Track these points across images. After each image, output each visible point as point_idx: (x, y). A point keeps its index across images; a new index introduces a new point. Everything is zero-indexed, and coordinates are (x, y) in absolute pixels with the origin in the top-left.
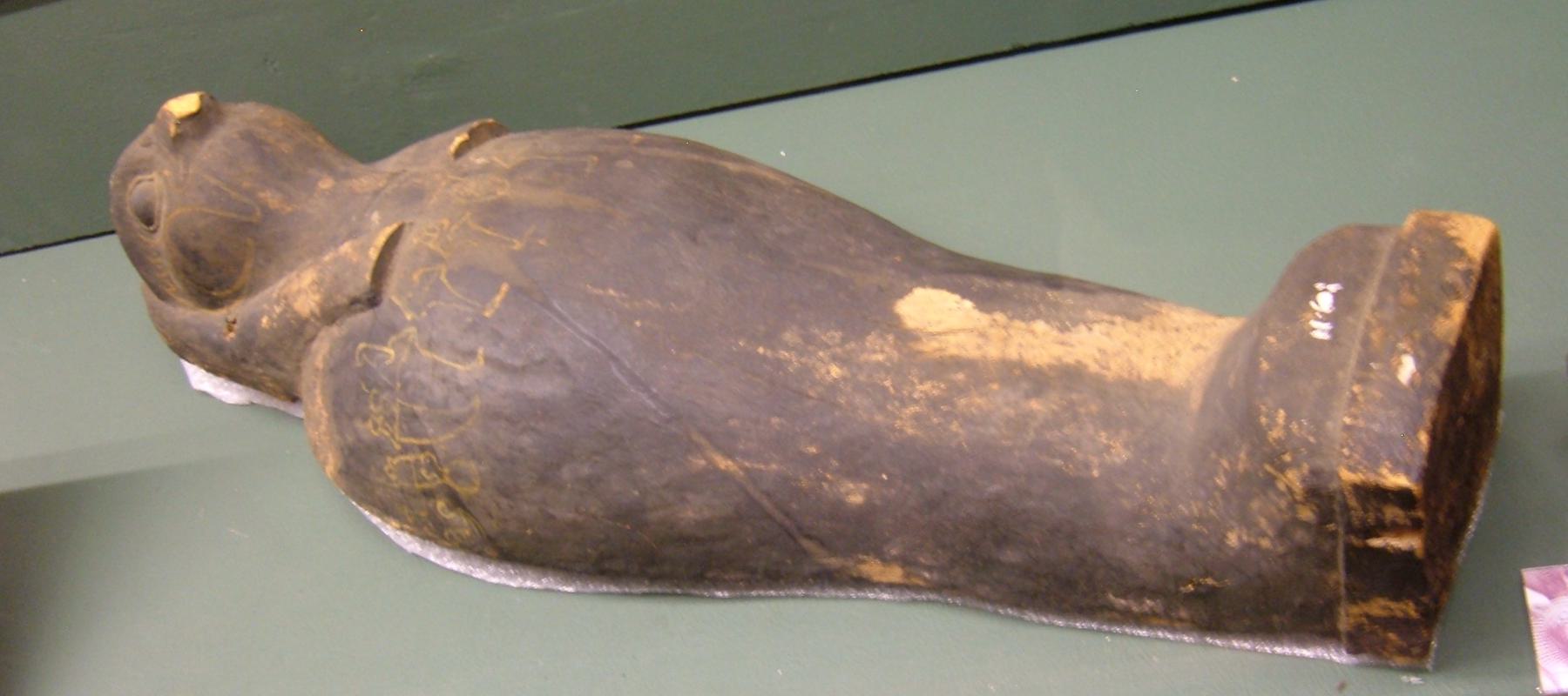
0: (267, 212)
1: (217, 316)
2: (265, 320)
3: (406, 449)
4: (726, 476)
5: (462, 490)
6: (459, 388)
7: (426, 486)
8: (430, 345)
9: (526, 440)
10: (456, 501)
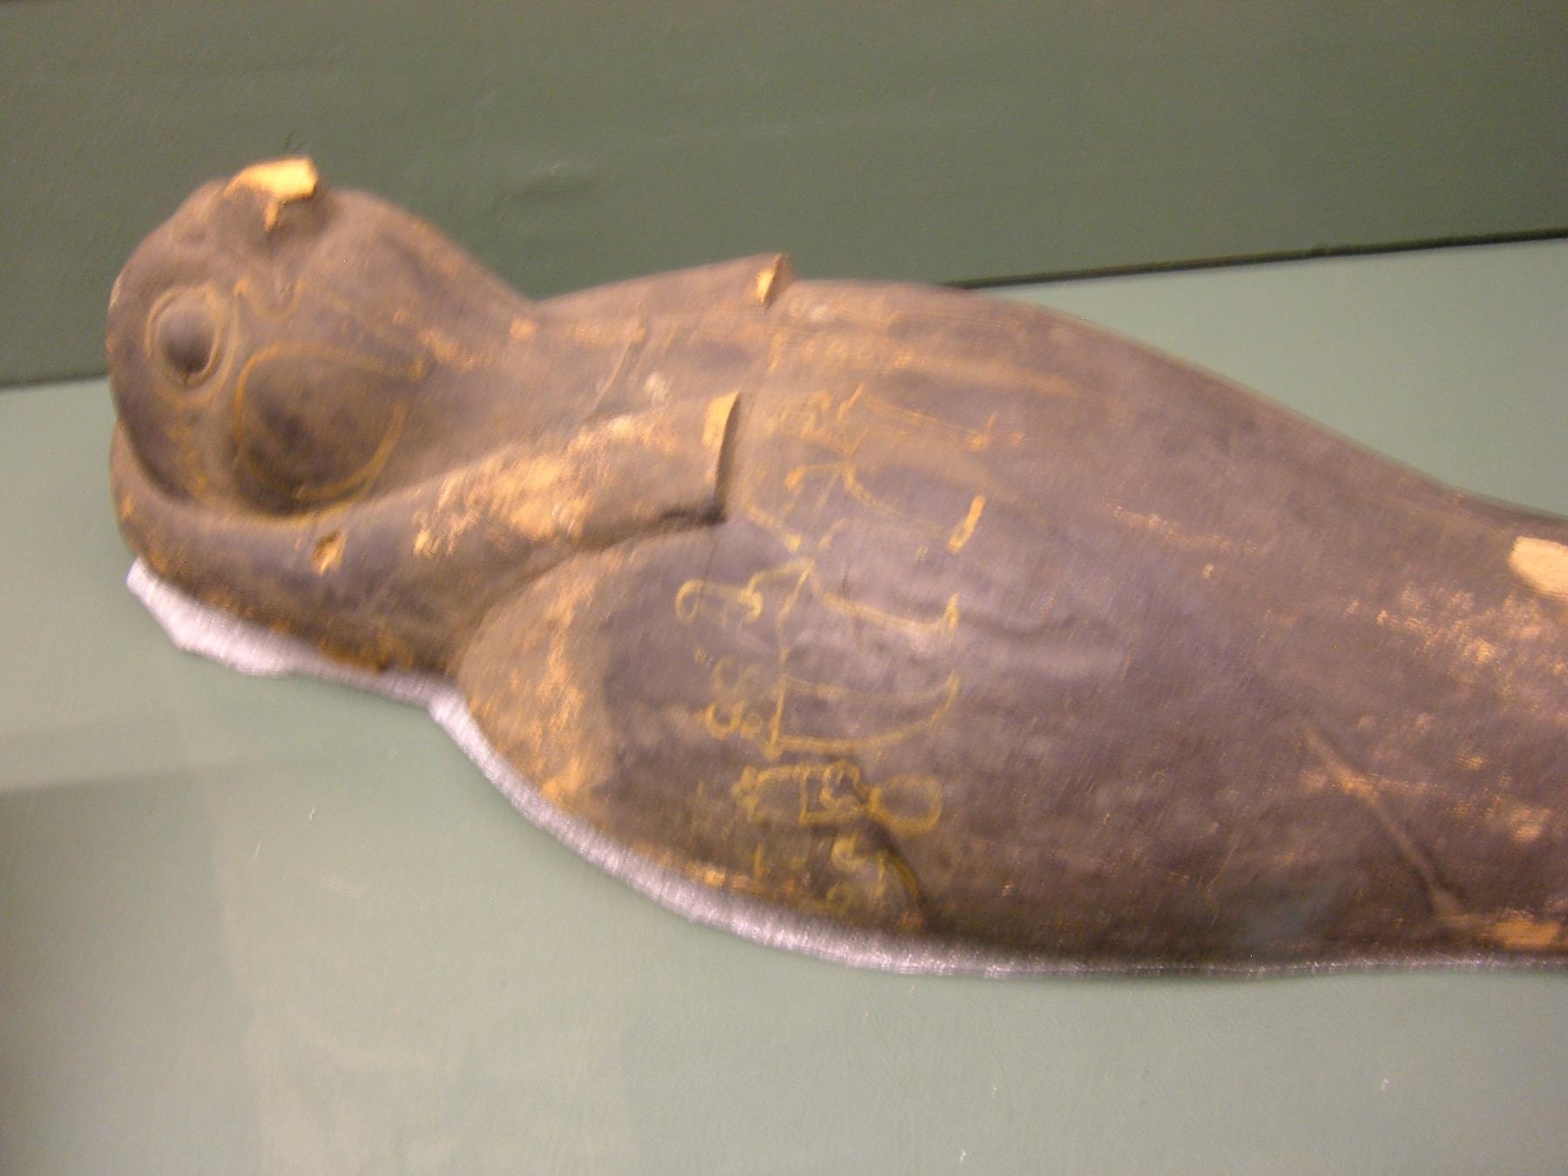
0: (433, 365)
1: (293, 531)
2: (422, 541)
3: (790, 758)
4: (1352, 802)
5: (899, 824)
6: (914, 661)
7: (824, 818)
8: (845, 590)
9: (1040, 746)
10: (880, 840)
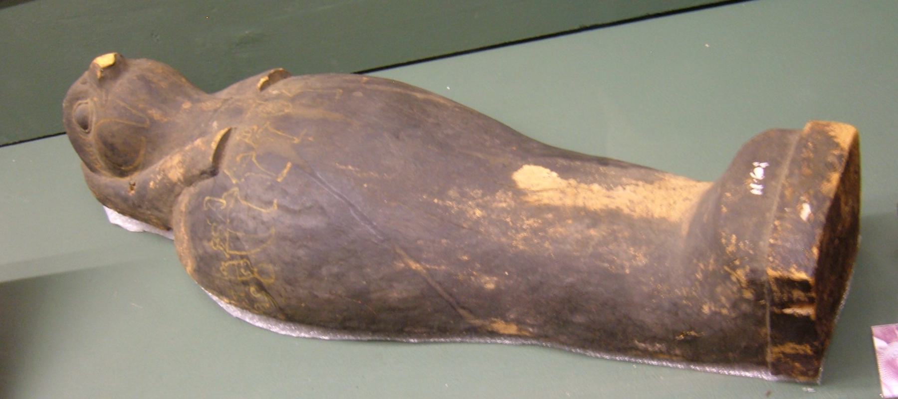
0: (153, 122)
1: (124, 181)
2: (152, 184)
3: (232, 258)
4: (416, 273)
5: (265, 281)
6: (263, 223)
7: (244, 278)
8: (246, 198)
9: (301, 252)
10: (261, 287)
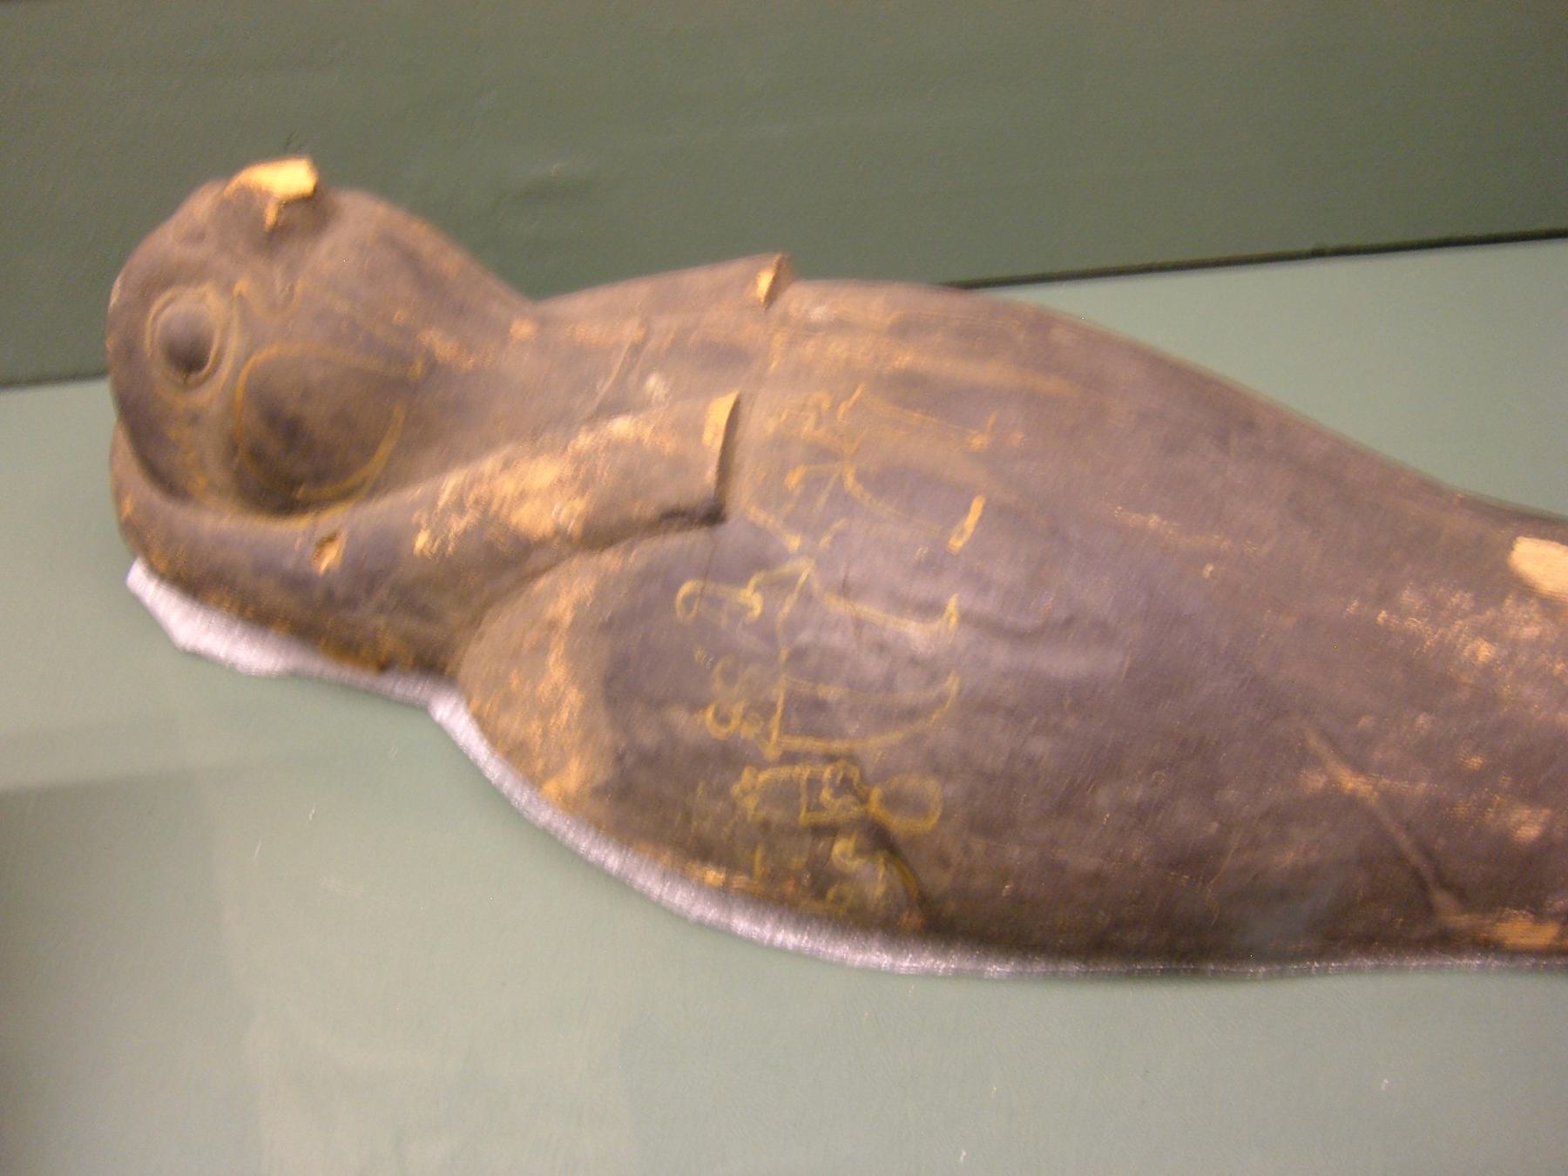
0: (433, 365)
1: (293, 531)
2: (422, 541)
3: (790, 758)
4: (1352, 802)
5: (899, 824)
6: (914, 661)
7: (824, 818)
8: (845, 590)
9: (1040, 746)
10: (880, 840)
